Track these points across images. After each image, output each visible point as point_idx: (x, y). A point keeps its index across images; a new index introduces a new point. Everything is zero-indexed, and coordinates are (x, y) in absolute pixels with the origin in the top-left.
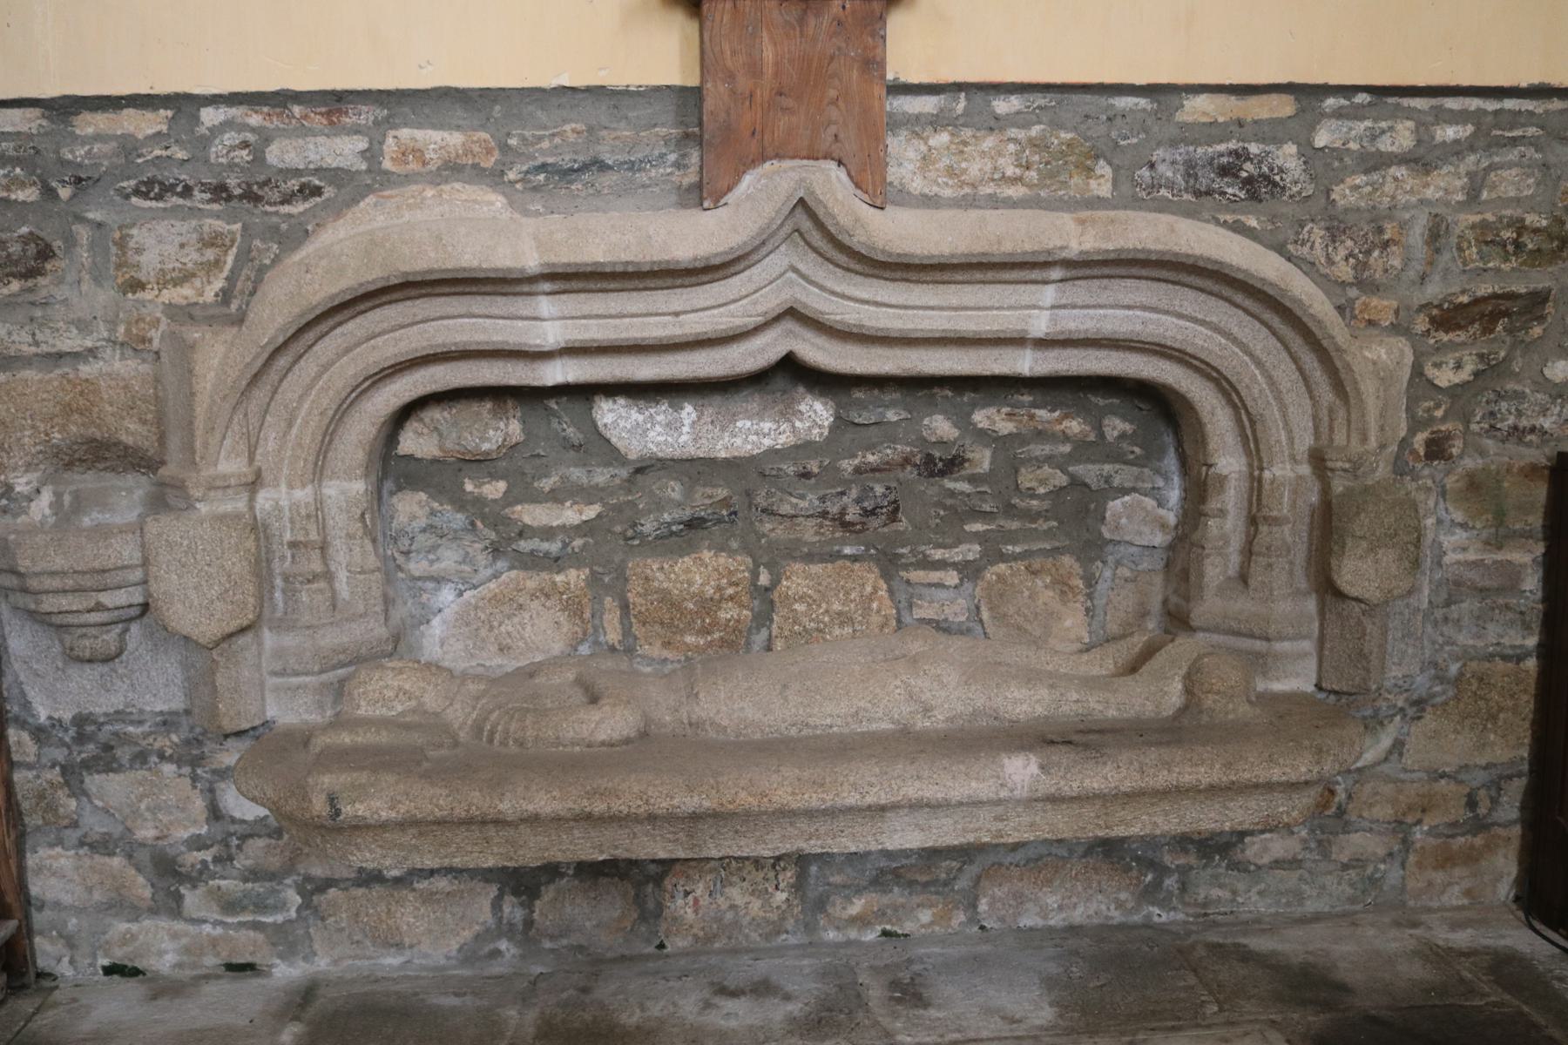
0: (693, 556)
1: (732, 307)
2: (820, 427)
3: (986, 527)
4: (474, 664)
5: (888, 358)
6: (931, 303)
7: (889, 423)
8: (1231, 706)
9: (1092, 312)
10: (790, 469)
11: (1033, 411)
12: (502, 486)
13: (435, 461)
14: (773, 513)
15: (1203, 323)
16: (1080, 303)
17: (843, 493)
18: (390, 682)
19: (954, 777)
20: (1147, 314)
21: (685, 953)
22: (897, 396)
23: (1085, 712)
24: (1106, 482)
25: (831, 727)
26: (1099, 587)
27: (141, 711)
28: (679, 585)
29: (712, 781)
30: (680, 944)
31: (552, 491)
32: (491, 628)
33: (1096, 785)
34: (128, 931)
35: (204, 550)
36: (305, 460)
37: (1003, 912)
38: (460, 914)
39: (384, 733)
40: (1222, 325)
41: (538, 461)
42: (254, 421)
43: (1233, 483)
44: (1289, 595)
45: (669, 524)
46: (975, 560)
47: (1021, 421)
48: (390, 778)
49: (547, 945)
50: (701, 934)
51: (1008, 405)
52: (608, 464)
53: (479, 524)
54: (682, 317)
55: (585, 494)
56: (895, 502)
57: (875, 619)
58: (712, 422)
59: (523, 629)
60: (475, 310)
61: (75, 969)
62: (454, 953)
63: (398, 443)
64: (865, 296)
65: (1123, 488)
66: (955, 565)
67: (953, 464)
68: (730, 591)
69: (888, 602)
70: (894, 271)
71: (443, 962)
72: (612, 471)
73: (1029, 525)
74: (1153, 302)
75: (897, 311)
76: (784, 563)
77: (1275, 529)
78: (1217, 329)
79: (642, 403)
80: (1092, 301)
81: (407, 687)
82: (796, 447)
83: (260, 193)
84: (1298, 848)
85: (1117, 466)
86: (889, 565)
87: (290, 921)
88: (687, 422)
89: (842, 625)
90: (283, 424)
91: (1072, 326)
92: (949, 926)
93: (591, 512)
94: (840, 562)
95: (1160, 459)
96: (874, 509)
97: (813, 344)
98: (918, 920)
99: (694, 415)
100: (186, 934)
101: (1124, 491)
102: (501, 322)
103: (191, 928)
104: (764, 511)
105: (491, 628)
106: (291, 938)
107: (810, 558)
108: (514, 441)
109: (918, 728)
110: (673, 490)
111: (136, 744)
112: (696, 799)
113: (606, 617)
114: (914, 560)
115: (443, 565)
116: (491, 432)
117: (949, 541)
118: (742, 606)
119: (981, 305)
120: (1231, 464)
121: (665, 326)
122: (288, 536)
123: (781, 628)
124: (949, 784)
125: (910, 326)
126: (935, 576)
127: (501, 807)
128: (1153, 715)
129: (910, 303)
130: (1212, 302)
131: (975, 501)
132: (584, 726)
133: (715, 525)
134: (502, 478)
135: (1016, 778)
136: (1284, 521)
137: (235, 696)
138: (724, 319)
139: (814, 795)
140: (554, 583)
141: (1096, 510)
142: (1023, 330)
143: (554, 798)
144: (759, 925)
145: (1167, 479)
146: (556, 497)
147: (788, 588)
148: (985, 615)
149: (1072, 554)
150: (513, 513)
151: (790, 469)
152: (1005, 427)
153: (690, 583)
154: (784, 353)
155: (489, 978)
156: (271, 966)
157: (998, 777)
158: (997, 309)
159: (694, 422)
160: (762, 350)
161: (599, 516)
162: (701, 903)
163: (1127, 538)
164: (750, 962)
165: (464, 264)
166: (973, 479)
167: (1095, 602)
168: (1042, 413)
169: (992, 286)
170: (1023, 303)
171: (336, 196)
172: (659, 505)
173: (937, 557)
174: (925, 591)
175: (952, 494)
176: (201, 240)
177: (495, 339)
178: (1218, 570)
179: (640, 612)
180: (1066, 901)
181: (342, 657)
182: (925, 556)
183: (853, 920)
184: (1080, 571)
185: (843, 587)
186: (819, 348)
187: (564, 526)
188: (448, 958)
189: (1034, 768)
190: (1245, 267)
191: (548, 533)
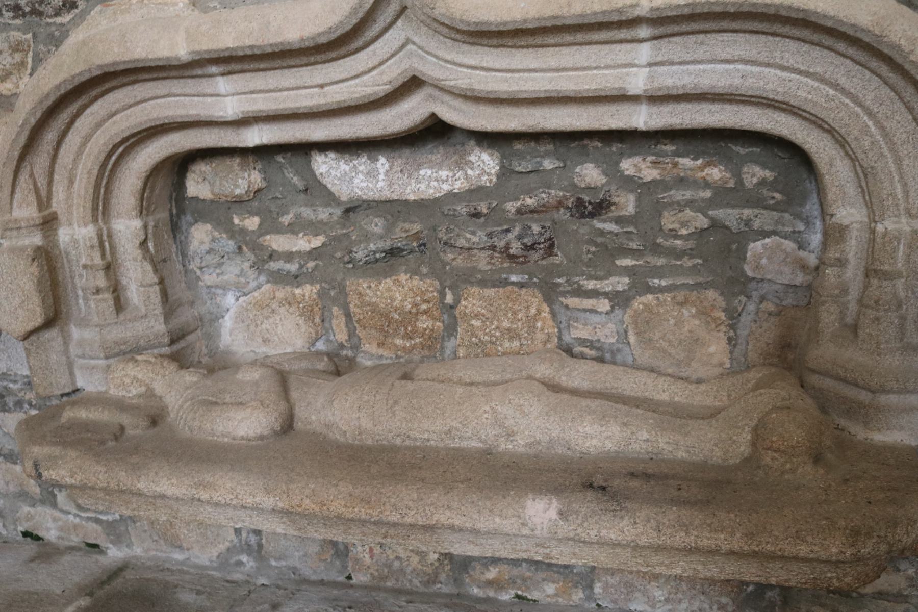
0: (394, 278)
1: (365, 78)
2: (488, 174)
3: (634, 262)
4: (249, 350)
5: (515, 116)
6: (532, 66)
7: (544, 171)
8: (788, 466)
9: (691, 67)
10: (462, 209)
11: (677, 159)
12: (256, 220)
13: (212, 201)
14: (452, 246)
15: (807, 74)
16: (677, 60)
17: (508, 231)
18: (129, 372)
19: (479, 512)
20: (748, 68)
21: (364, 587)
22: (550, 147)
23: (655, 451)
24: (746, 225)
25: (428, 440)
26: (743, 319)
27: (16, 375)
28: (384, 301)
29: (284, 488)
30: (362, 579)
31: (289, 225)
32: (257, 325)
33: (613, 536)
34: (29, 513)
35: (6, 273)
36: (84, 206)
37: (616, 596)
38: (216, 533)
39: (106, 412)
40: (827, 76)
41: (279, 202)
42: (42, 182)
43: (854, 233)
44: (898, 349)
45: (375, 253)
46: (624, 291)
47: (665, 169)
48: (73, 454)
49: (274, 563)
50: (376, 574)
51: (653, 154)
52: (327, 205)
53: (244, 248)
54: (326, 89)
55: (313, 228)
56: (550, 239)
57: (540, 336)
58: (402, 171)
59: (276, 327)
60: (175, 90)
61: (7, 530)
62: (214, 559)
63: (186, 188)
64: (472, 62)
65: (763, 231)
66: (606, 295)
67: (601, 207)
68: (424, 307)
69: (550, 323)
70: (489, 38)
71: (207, 563)
72: (331, 210)
73: (673, 262)
74: (752, 54)
75: (505, 75)
76: (463, 286)
77: (885, 283)
78: (822, 80)
79: (347, 156)
80: (688, 57)
81: (140, 376)
82: (470, 191)
83: (41, 9)
84: (904, 584)
85: (756, 211)
86: (550, 293)
87: (115, 521)
88: (382, 171)
89: (511, 339)
90: (66, 181)
91: (669, 82)
92: (570, 600)
93: (317, 242)
94: (509, 288)
95: (802, 204)
96: (533, 244)
97: (450, 106)
98: (544, 591)
99: (387, 166)
100: (60, 519)
101: (764, 234)
102: (196, 99)
103: (62, 516)
104: (445, 243)
105: (257, 325)
106: (118, 532)
107: (483, 283)
108: (256, 187)
109: (500, 450)
110: (376, 225)
111: (16, 395)
112: (272, 499)
113: (334, 322)
114: (569, 288)
115: (226, 278)
116: (240, 181)
117: (601, 273)
118: (434, 319)
119: (579, 65)
120: (852, 215)
121: (312, 96)
122: (83, 261)
123: (462, 339)
124: (475, 516)
125: (515, 88)
126: (588, 303)
127: (139, 486)
128: (720, 461)
129: (513, 67)
130: (817, 52)
131: (623, 240)
132: (230, 423)
133: (409, 253)
134: (257, 214)
135: (537, 520)
136: (900, 275)
137: (47, 372)
138: (359, 89)
139: (363, 510)
140: (294, 294)
141: (738, 249)
142: (621, 88)
143: (173, 484)
144: (418, 574)
145: (808, 223)
146: (293, 229)
147: (466, 307)
148: (632, 339)
149: (716, 288)
150: (265, 241)
151: (462, 209)
152: (650, 174)
153: (393, 299)
154: (427, 115)
155: (228, 581)
156: (107, 548)
157: (519, 517)
158: (596, 68)
159: (387, 171)
160: (408, 113)
161: (324, 245)
162: (375, 551)
163: (769, 277)
164: (404, 604)
165: (137, 57)
166: (619, 221)
167: (739, 332)
168: (686, 162)
169: (587, 47)
170: (619, 62)
171: (86, 8)
172: (367, 237)
173: (590, 287)
174: (582, 315)
175: (602, 233)
176: (10, 47)
177: (191, 112)
178: (833, 317)
179: (359, 320)
180: (672, 596)
181: (123, 347)
182: (580, 286)
183: (490, 583)
184: (723, 304)
185: (511, 308)
186: (455, 109)
187: (300, 252)
188: (211, 561)
189: (553, 514)
190: (832, 14)
191: (289, 256)
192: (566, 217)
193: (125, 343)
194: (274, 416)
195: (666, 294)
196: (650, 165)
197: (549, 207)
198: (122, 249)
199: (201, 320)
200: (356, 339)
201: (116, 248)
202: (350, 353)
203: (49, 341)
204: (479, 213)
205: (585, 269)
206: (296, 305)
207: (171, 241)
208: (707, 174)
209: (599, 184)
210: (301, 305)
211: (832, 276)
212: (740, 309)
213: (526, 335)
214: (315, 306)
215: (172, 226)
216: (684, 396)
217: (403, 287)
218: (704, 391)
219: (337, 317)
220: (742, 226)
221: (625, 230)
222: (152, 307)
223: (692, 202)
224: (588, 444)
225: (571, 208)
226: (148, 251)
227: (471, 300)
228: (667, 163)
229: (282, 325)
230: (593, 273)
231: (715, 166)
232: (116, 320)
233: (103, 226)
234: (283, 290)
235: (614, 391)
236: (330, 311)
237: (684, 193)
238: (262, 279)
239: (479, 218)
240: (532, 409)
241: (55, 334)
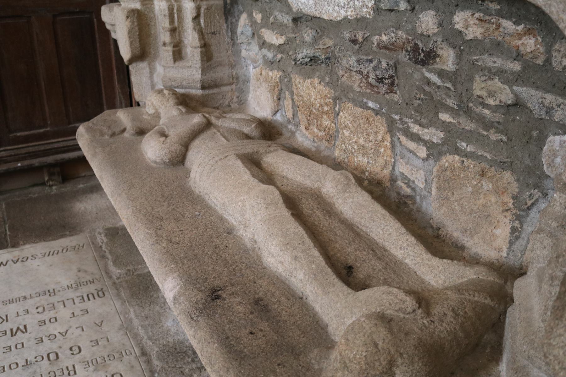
3: (451, 120)
7: (398, 11)
24: (547, 113)
46: (438, 145)
51: (480, 11)
113: (285, 101)
114: (401, 126)
126: (412, 145)
166: (441, 74)
167: (525, 226)
168: (508, 24)
175: (429, 83)
181: (173, 83)
182: (408, 127)
192: (406, 59)
193: (175, 81)
194: (165, 151)
195: (470, 160)
196: (477, 22)
197: (396, 47)
198: (187, 20)
199: (237, 79)
201: (184, 19)
202: (293, 128)
203: (142, 69)
204: (357, 40)
205: (413, 113)
207: (222, 21)
208: (523, 44)
209: (430, 33)
211: (558, 204)
212: (529, 203)
213: (372, 155)
214: (276, 87)
215: (225, 11)
216: (414, 262)
217: (315, 88)
218: (432, 266)
220: (543, 112)
221: (445, 85)
223: (502, 72)
224: (269, 260)
225: (410, 52)
226: (199, 24)
227: (345, 112)
228: (493, 23)
230: (418, 118)
231: (534, 36)
232: (173, 65)
233: (174, 3)
235: (364, 229)
237: (495, 59)
239: (355, 45)
240: (258, 213)
241: (145, 65)
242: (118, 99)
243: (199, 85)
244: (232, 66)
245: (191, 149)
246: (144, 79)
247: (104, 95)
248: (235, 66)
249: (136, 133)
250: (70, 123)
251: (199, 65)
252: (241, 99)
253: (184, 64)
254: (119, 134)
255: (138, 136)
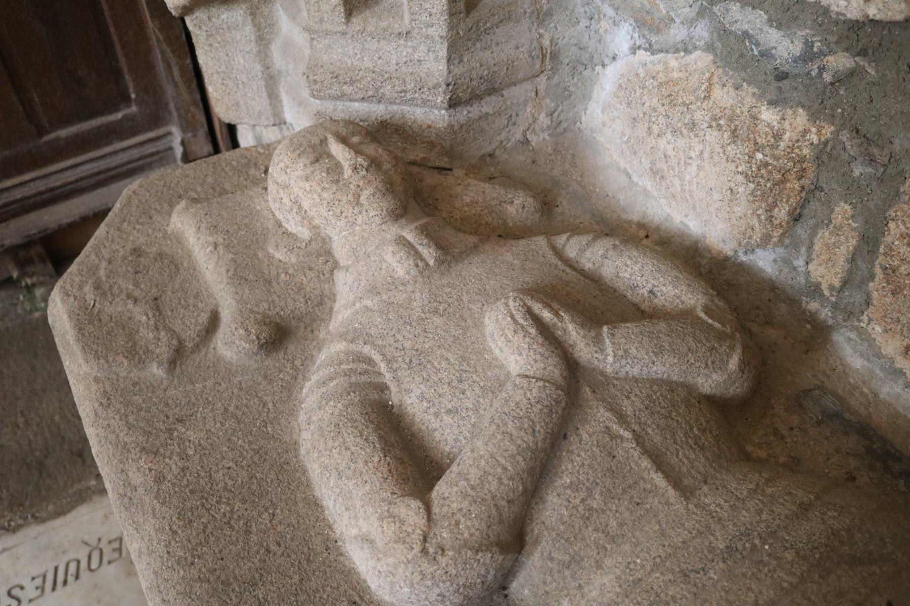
4: (623, 165)
193: (352, 82)
194: (437, 591)
199: (555, 56)
200: (859, 297)
202: (825, 314)
203: (229, 28)
206: (748, 147)
210: (759, 156)
214: (792, 176)
219: (838, 228)
222: (424, 18)
229: (699, 167)
234: (732, 93)
236: (829, 207)
238: (702, 31)
242: (159, 57)
243: (441, 99)
244: (541, 17)
245: (536, 542)
246: (240, 61)
247: (118, 47)
248: (549, 14)
249: (261, 347)
250: (41, 132)
251: (439, 29)
252: (561, 118)
253: (384, 24)
254: (197, 347)
255: (268, 354)
